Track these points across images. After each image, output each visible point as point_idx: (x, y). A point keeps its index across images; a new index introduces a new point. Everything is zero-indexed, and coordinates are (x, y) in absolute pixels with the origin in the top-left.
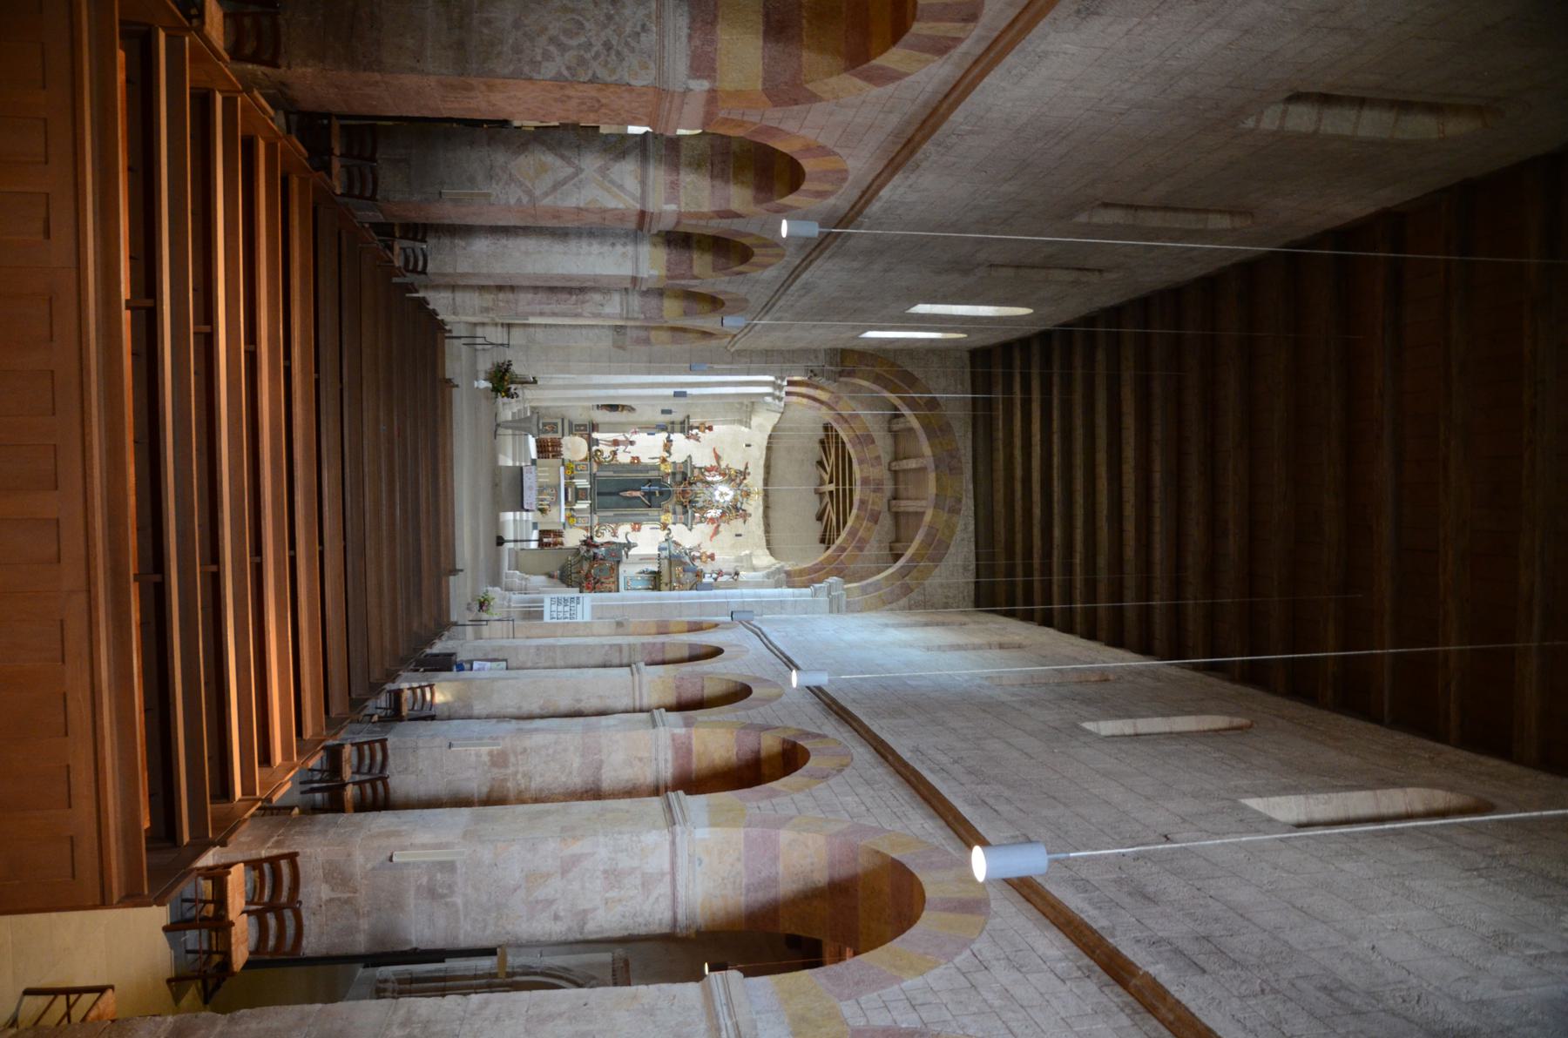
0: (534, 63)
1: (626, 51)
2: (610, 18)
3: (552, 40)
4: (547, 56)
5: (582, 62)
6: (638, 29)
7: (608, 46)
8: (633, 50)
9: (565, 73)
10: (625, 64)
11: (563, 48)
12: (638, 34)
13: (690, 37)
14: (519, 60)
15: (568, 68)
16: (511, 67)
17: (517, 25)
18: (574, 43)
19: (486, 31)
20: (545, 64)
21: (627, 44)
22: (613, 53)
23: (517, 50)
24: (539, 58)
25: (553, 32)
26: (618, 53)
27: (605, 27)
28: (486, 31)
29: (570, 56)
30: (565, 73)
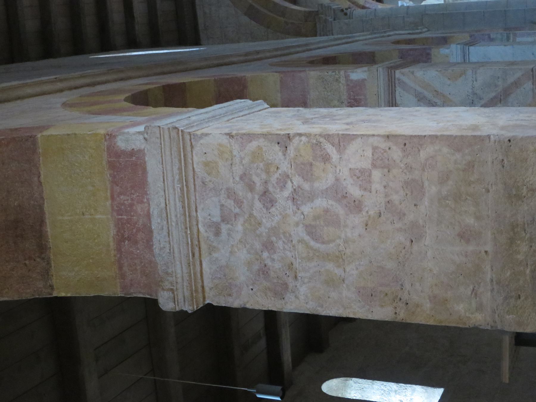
0: (381, 162)
1: (240, 190)
2: (269, 246)
3: (357, 206)
4: (362, 177)
5: (306, 171)
6: (224, 228)
7: (267, 199)
8: (231, 194)
9: (331, 150)
10: (238, 170)
11: (337, 192)
12: (224, 219)
13: (148, 216)
14: (409, 168)
15: (326, 159)
16: (423, 155)
17: (415, 233)
18: (321, 203)
19: (470, 221)
20: (366, 164)
21: (239, 203)
22: (259, 187)
23: (414, 188)
24: (377, 174)
25: (356, 220)
26: (251, 187)
27: (274, 230)
28: (470, 221)
29: (325, 181)
30: (331, 150)
